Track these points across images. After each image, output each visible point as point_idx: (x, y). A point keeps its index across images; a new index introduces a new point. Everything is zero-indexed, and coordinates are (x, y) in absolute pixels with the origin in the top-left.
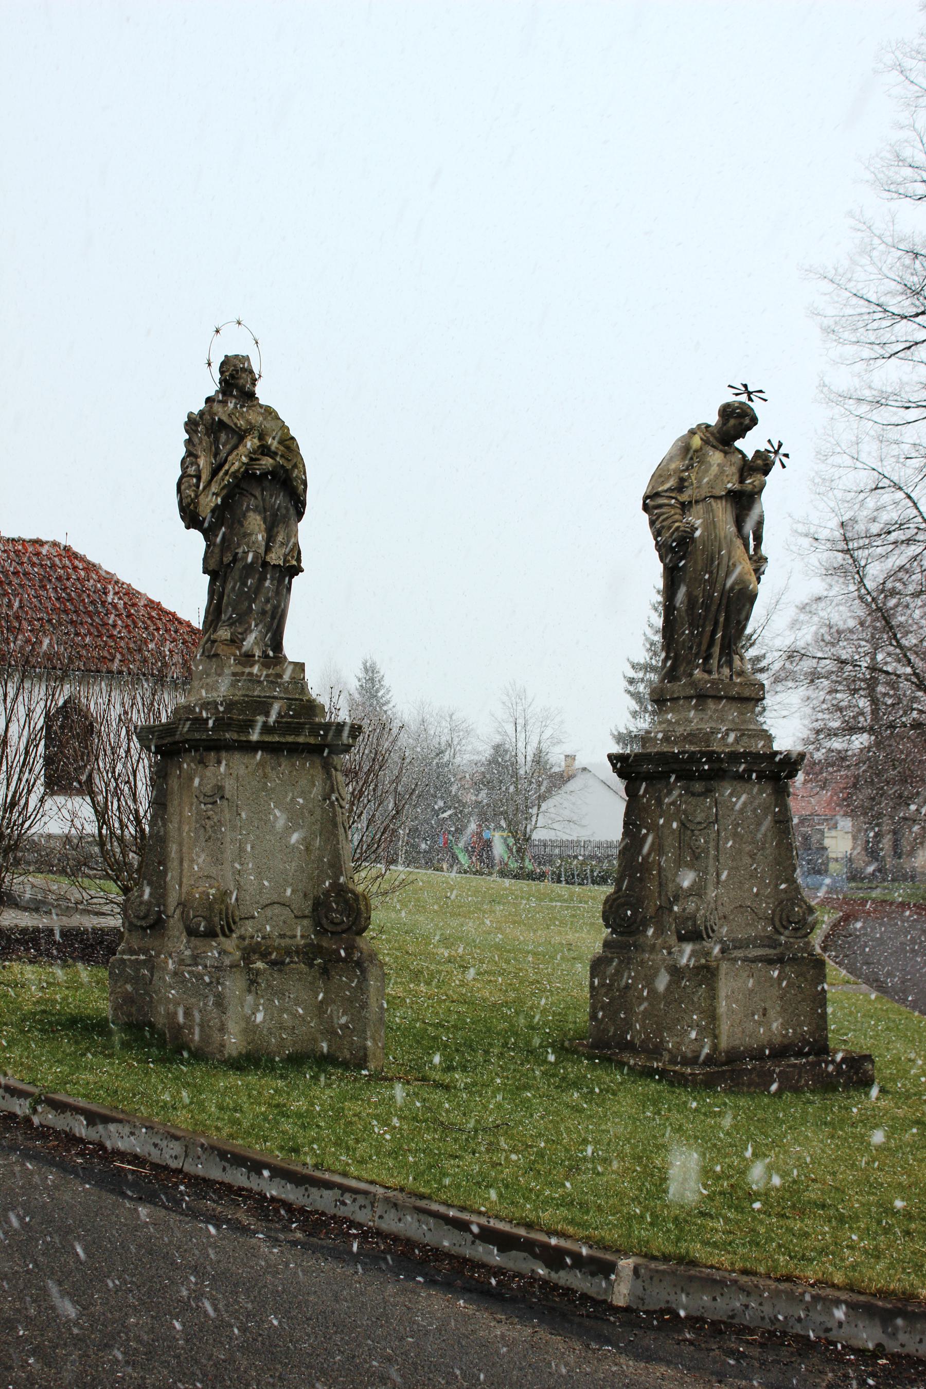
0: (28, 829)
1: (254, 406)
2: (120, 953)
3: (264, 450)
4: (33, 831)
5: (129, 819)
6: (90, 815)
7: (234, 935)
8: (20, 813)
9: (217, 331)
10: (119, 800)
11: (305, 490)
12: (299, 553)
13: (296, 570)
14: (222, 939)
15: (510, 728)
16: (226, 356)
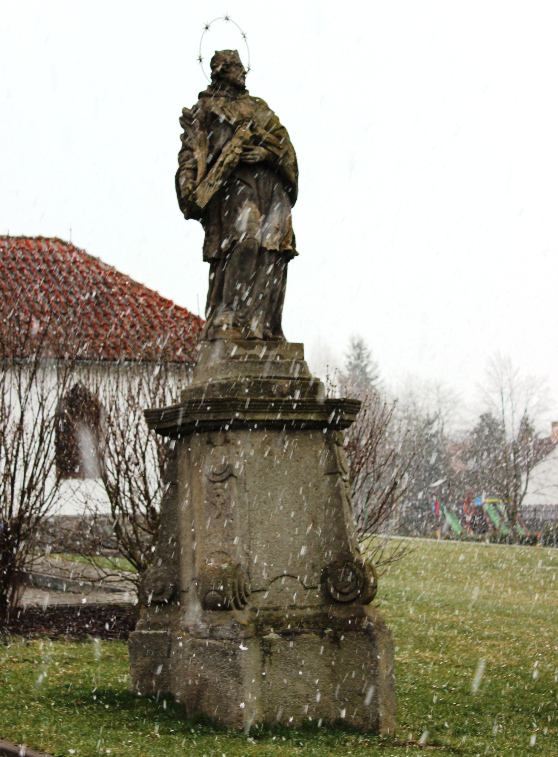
0: (45, 512)
1: (245, 98)
2: (139, 629)
3: (256, 140)
4: (48, 514)
5: (140, 499)
6: (103, 496)
7: (247, 608)
8: (37, 497)
9: (207, 28)
10: (130, 482)
11: (297, 178)
12: (294, 238)
13: (291, 254)
14: (235, 612)
15: (496, 398)
16: (216, 52)
